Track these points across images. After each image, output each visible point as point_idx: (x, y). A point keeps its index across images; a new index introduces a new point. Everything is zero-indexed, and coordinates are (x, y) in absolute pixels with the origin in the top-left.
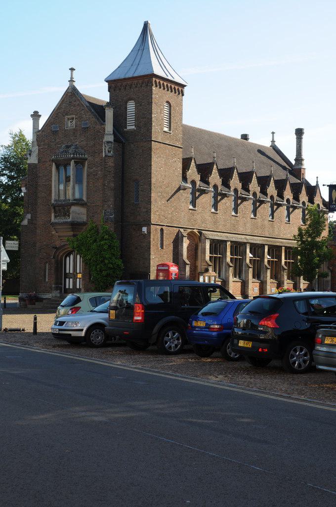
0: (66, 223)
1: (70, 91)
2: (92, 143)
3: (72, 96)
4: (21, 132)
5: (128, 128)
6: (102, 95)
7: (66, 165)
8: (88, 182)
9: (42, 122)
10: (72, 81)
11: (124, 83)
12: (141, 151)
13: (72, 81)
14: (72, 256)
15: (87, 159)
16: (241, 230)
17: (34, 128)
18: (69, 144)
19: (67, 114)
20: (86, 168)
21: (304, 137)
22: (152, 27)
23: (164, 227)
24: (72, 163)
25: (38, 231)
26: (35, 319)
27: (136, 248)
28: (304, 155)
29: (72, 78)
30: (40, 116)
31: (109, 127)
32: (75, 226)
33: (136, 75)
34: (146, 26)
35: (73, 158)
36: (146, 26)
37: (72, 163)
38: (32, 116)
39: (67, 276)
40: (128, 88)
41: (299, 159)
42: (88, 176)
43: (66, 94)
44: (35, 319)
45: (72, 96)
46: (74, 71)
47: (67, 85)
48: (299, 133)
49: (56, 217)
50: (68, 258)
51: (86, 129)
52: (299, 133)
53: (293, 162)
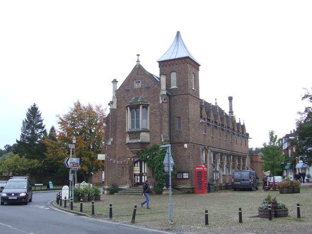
0: (138, 143)
1: (137, 67)
2: (152, 96)
3: (139, 71)
4: (78, 101)
5: (172, 87)
6: (155, 71)
7: (137, 107)
8: (150, 118)
9: (119, 85)
10: (138, 61)
11: (169, 63)
12: (181, 100)
13: (138, 61)
14: (139, 163)
15: (149, 105)
16: (222, 147)
17: (114, 89)
18: (137, 97)
19: (135, 80)
20: (149, 110)
21: (233, 101)
22: (181, 33)
23: (195, 145)
24: (141, 107)
25: (117, 148)
26: (93, 207)
27: (180, 157)
28: (234, 110)
29: (138, 60)
30: (117, 82)
31: (163, 87)
32: (143, 144)
33: (177, 57)
34: (178, 33)
35: (141, 104)
36: (178, 33)
37: (141, 107)
38: (112, 82)
39: (135, 175)
40: (171, 65)
41: (231, 112)
42: (150, 114)
43: (135, 68)
44: (93, 207)
45: (139, 71)
46: (139, 56)
47: (136, 63)
48: (230, 99)
49: (130, 139)
50: (136, 164)
51: (148, 88)
52: (230, 99)
53: (228, 114)
